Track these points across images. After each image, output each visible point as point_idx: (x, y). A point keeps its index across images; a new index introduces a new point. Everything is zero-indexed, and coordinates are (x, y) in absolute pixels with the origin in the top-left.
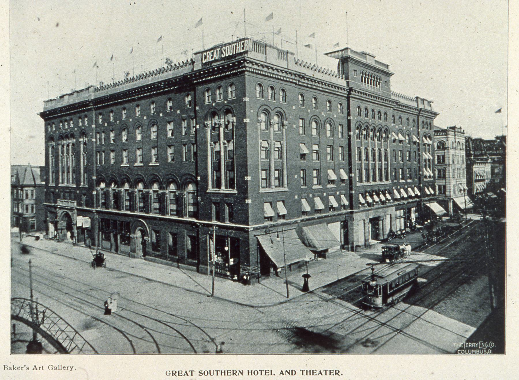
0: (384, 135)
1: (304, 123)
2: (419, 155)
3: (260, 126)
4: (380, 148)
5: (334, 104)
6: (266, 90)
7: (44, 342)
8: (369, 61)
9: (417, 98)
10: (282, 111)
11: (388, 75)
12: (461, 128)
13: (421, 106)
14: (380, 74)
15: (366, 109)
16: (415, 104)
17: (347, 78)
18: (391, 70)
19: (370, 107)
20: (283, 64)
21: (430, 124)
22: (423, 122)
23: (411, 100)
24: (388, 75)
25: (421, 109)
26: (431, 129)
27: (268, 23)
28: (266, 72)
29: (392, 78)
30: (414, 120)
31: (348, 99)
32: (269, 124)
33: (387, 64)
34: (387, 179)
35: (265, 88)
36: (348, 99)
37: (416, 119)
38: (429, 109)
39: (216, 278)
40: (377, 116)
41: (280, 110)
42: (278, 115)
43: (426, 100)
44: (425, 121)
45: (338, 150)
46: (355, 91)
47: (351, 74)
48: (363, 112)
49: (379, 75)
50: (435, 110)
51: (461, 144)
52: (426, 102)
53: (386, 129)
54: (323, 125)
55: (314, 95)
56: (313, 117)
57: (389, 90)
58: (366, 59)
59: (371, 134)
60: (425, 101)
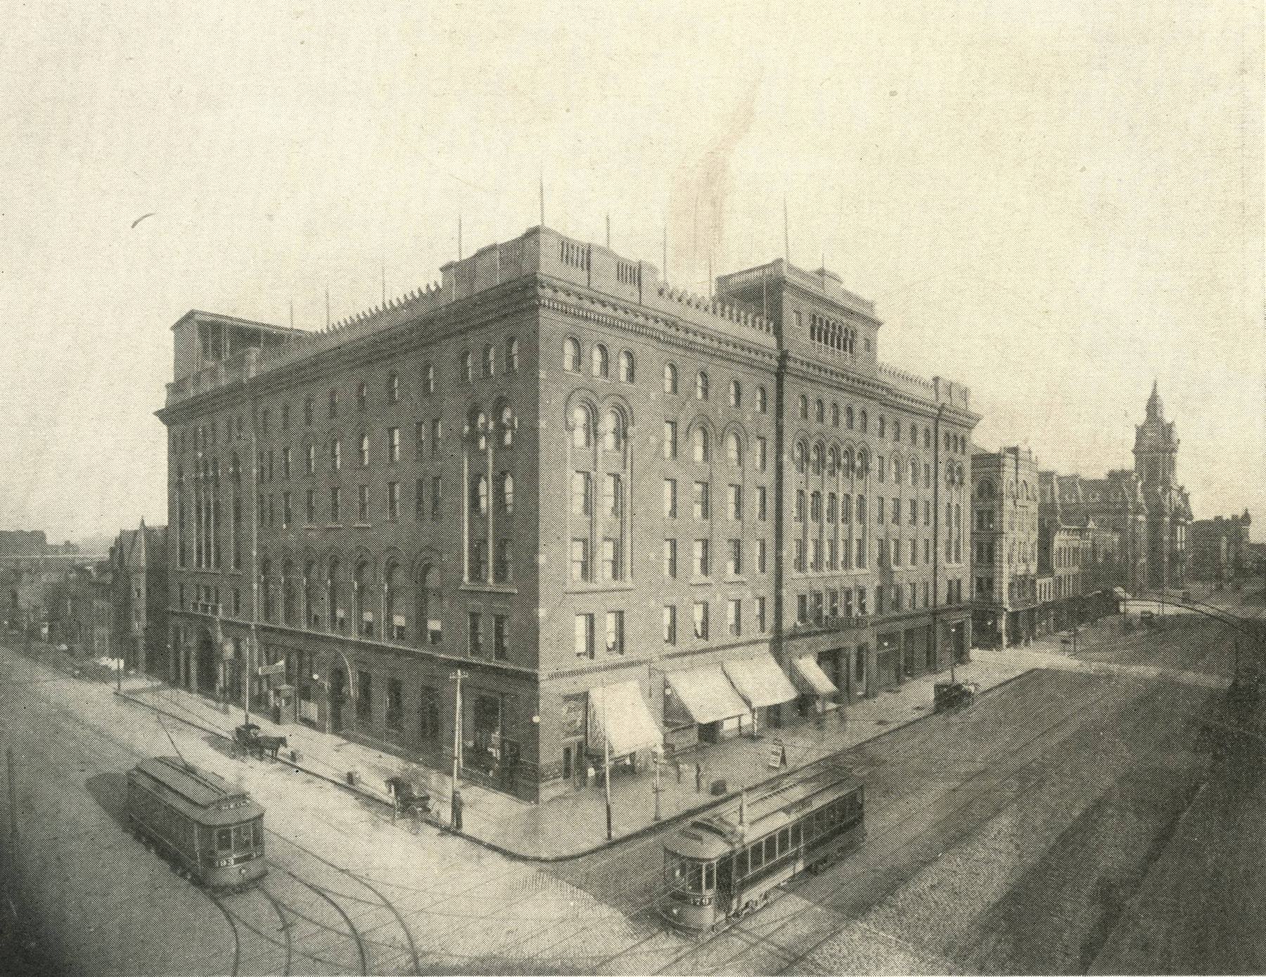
0: (813, 456)
1: (675, 433)
2: (406, 351)
3: (573, 439)
4: (834, 491)
5: (746, 389)
6: (587, 353)
7: (817, 276)
8: (831, 292)
10: (626, 408)
11: (878, 324)
14: (843, 326)
15: (820, 402)
16: (929, 396)
17: (778, 332)
18: (879, 315)
19: (828, 396)
20: (627, 292)
21: (963, 440)
22: (947, 435)
23: (925, 385)
26: (963, 453)
27: (637, 382)
28: (586, 309)
30: (927, 431)
31: (780, 376)
32: (592, 432)
34: (861, 564)
35: (586, 348)
36: (780, 376)
38: (962, 405)
40: (843, 419)
41: (621, 401)
44: (952, 432)
46: (795, 360)
47: (789, 318)
48: (813, 409)
49: (852, 323)
51: (1030, 487)
53: (863, 450)
57: (873, 360)
59: (829, 459)
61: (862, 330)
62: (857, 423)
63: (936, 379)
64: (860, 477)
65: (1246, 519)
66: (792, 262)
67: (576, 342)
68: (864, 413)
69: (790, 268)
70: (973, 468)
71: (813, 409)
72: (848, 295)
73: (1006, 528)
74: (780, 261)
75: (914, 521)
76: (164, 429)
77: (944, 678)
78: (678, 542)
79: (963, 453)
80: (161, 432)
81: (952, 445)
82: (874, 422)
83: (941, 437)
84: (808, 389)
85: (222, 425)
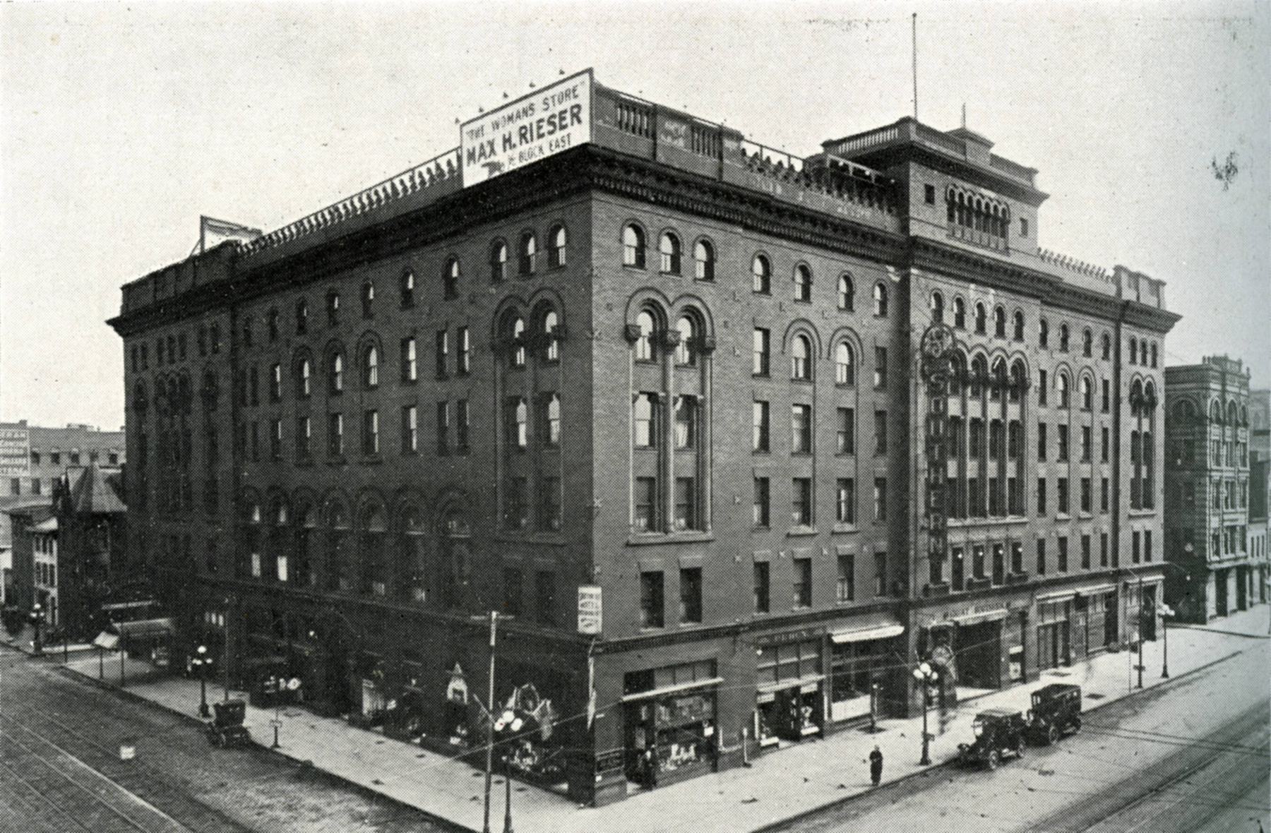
9: (1118, 269)
11: (1037, 198)
12: (1239, 363)
13: (1129, 295)
15: (960, 302)
16: (1111, 291)
18: (1041, 183)
20: (705, 166)
21: (1154, 347)
24: (1037, 198)
25: (1128, 302)
29: (1044, 209)
33: (1026, 164)
37: (1112, 333)
39: (1169, 631)
41: (653, 296)
42: (688, 318)
43: (1146, 278)
45: (344, 382)
50: (1170, 306)
52: (1143, 285)
54: (825, 348)
55: (957, 293)
56: (797, 326)
58: (964, 154)
60: (1141, 280)
61: (1017, 209)
62: (1010, 328)
63: (1118, 269)
64: (1015, 398)
65: (109, 322)
66: (922, 120)
67: (638, 231)
68: (1065, 328)
69: (921, 128)
70: (1167, 383)
71: (1054, 336)
72: (996, 160)
73: (1210, 463)
74: (905, 121)
75: (1087, 457)
76: (119, 341)
77: (1047, 679)
78: (772, 482)
79: (1154, 365)
80: (116, 343)
81: (1139, 355)
82: (1076, 338)
83: (1125, 344)
84: (949, 288)
85: (192, 337)
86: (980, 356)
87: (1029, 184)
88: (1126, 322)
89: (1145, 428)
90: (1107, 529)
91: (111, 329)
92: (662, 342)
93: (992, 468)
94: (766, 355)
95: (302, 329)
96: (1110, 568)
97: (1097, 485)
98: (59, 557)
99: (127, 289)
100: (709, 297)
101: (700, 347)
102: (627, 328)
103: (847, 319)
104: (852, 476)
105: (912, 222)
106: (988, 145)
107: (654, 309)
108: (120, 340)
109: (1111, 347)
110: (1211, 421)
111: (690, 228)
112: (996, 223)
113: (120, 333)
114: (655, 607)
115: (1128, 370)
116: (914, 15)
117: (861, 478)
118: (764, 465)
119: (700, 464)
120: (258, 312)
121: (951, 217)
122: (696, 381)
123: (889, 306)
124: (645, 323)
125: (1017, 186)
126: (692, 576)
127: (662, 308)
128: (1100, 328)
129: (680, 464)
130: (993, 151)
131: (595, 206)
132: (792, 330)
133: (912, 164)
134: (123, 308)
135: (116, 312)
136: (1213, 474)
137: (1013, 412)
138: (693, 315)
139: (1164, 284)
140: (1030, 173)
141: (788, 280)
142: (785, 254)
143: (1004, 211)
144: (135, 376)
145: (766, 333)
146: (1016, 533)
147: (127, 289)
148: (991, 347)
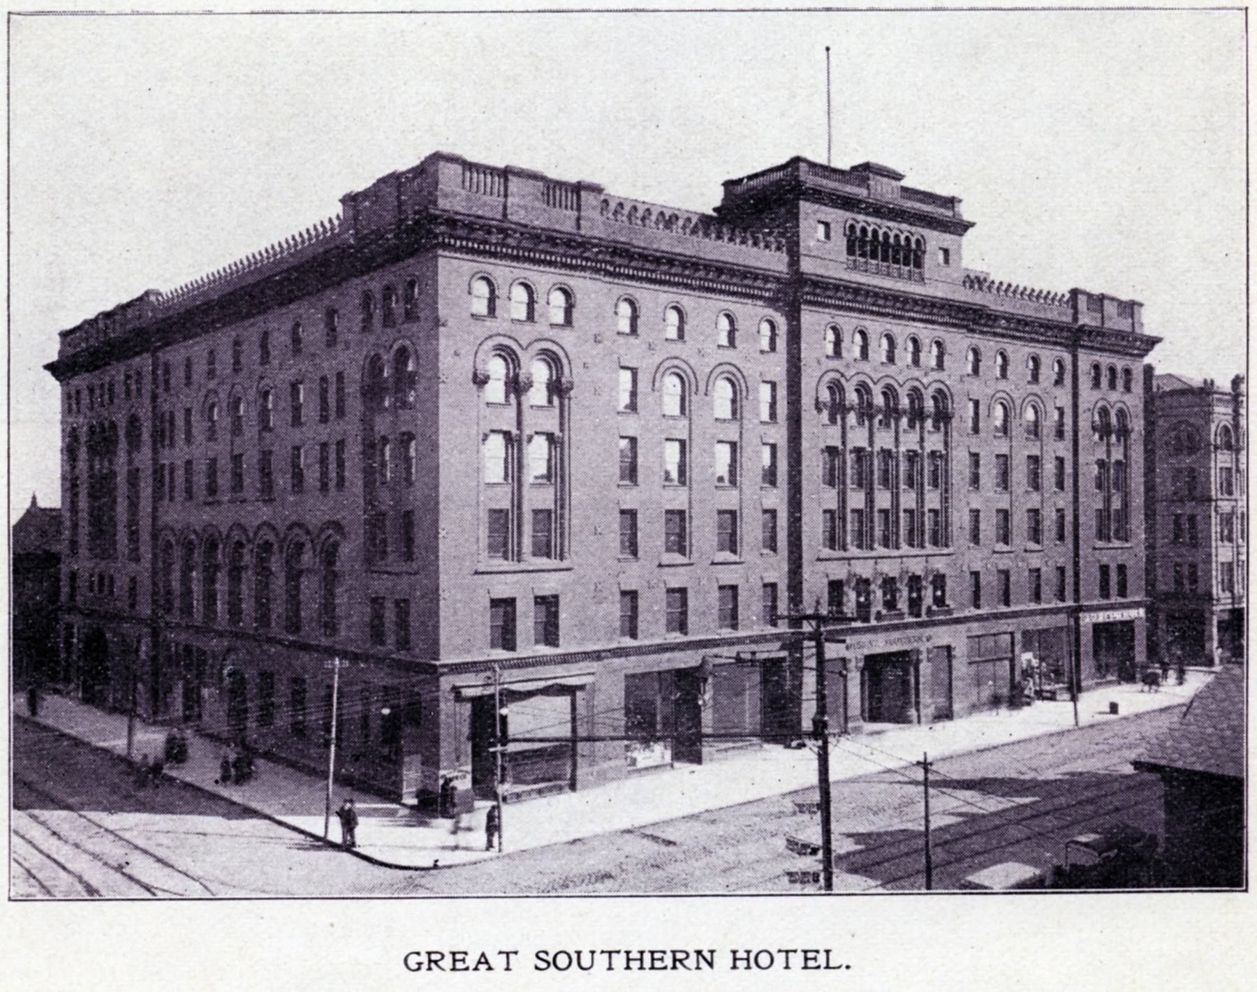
18: (966, 212)
24: (961, 227)
43: (1113, 299)
52: (1110, 309)
74: (796, 160)
86: (889, 387)
87: (950, 213)
88: (1083, 347)
89: (1117, 455)
90: (1064, 560)
91: (48, 374)
92: (516, 386)
93: (883, 499)
94: (634, 394)
95: (211, 374)
96: (1070, 603)
97: (179, 496)
98: (494, 716)
99: (64, 335)
100: (567, 338)
101: (557, 389)
102: (475, 375)
103: (729, 355)
104: (736, 507)
105: (802, 258)
106: (897, 177)
107: (508, 355)
108: (58, 383)
109: (1066, 376)
110: (1216, 448)
111: (544, 278)
112: (911, 256)
113: (57, 378)
114: (506, 636)
115: (1088, 396)
116: (828, 49)
117: (745, 511)
118: (630, 499)
119: (561, 501)
120: (175, 355)
121: (851, 251)
122: (557, 421)
123: (778, 341)
124: (497, 369)
125: (943, 215)
126: (549, 604)
127: (514, 352)
128: (1049, 355)
129: (539, 498)
130: (904, 183)
131: (441, 261)
132: (662, 369)
133: (802, 203)
134: (60, 352)
135: (53, 357)
136: (1219, 503)
137: (934, 442)
138: (552, 359)
139: (1141, 305)
140: (951, 202)
141: (659, 320)
142: (654, 299)
143: (918, 241)
144: (70, 420)
145: (634, 372)
146: (940, 565)
147: (64, 335)
148: (876, 376)
